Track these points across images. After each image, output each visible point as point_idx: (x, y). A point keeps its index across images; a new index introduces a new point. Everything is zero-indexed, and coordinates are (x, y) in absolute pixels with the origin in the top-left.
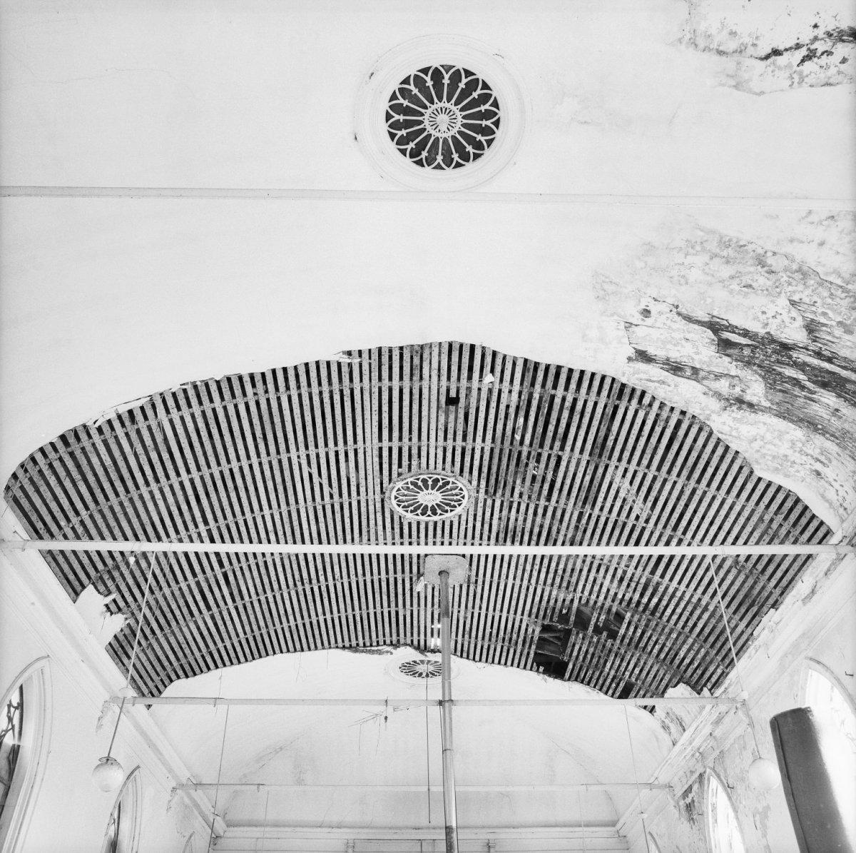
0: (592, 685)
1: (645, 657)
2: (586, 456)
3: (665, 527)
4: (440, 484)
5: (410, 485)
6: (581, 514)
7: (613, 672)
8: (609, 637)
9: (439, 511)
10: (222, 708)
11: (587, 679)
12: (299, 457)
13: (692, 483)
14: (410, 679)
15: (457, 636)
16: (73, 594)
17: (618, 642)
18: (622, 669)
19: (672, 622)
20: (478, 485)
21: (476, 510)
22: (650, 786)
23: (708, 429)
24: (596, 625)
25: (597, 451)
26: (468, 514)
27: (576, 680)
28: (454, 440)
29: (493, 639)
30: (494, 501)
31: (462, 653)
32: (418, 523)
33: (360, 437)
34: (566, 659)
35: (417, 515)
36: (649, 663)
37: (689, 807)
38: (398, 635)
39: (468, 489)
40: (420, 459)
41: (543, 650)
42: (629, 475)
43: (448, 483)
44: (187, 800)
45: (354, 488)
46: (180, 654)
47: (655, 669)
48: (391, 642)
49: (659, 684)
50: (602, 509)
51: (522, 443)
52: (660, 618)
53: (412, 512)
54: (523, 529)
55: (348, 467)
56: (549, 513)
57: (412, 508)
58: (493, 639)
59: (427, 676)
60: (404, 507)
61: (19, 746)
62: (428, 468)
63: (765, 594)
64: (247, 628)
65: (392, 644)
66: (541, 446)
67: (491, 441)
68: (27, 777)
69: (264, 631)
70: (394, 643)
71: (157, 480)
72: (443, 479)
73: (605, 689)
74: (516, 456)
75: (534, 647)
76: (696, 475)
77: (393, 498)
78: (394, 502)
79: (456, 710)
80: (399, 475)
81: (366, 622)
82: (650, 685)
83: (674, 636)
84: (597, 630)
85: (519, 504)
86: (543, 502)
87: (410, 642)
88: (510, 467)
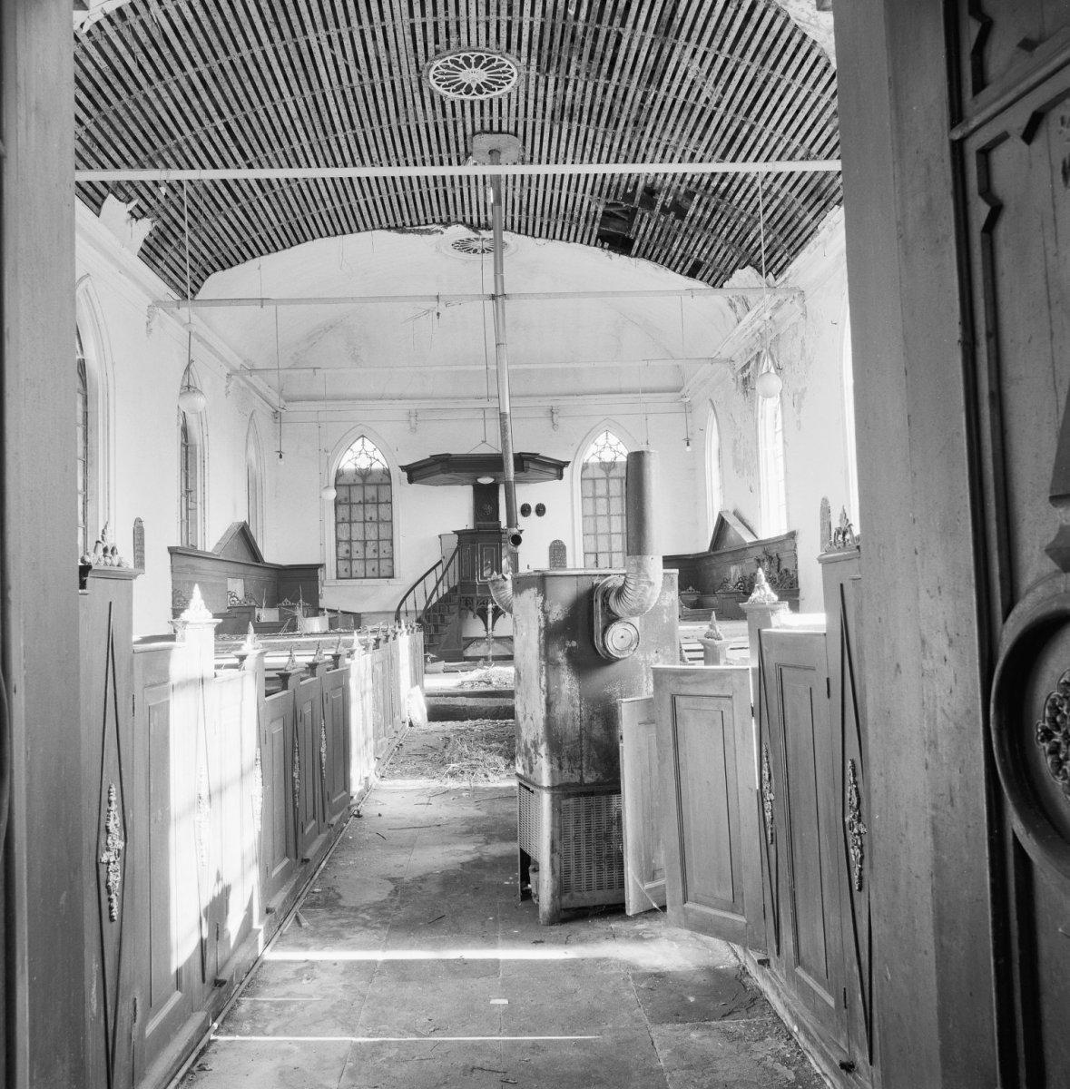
0: (660, 261)
1: (713, 239)
2: (650, 34)
3: (737, 111)
4: (485, 61)
5: (450, 64)
6: (645, 94)
7: (681, 251)
8: (677, 217)
9: (485, 90)
10: (269, 308)
11: (654, 257)
12: (318, 39)
13: (767, 69)
14: (464, 255)
15: (513, 212)
16: (95, 208)
17: (686, 222)
18: (691, 248)
19: (742, 207)
20: (529, 62)
21: (527, 87)
22: (712, 360)
23: (785, 14)
24: (663, 205)
25: (662, 29)
26: (518, 92)
27: (643, 256)
28: (498, 14)
29: (554, 216)
30: (547, 78)
31: (523, 229)
32: (463, 102)
33: (387, 15)
34: (632, 236)
35: (461, 94)
36: (718, 245)
37: (745, 381)
38: (448, 212)
39: (517, 71)
40: (460, 37)
41: (608, 227)
42: (698, 57)
43: (494, 60)
44: (242, 383)
45: (385, 69)
46: (214, 248)
47: (723, 250)
48: (441, 220)
49: (729, 263)
50: (668, 90)
51: (577, 17)
52: (731, 201)
53: (453, 91)
54: (582, 108)
55: (376, 47)
56: (610, 93)
57: (454, 87)
58: (554, 216)
59: (483, 251)
60: (444, 86)
61: (84, 360)
62: (469, 44)
63: (833, 189)
64: (282, 217)
65: (441, 222)
66: (599, 21)
67: (540, 15)
68: (100, 387)
69: (300, 218)
70: (444, 221)
71: (160, 77)
72: (487, 57)
73: (673, 266)
74: (570, 32)
75: (597, 224)
76: (771, 61)
77: (431, 77)
78: (433, 82)
79: (509, 305)
80: (437, 52)
81: (411, 203)
82: (719, 264)
83: (744, 220)
84: (664, 210)
85: (576, 81)
86: (602, 81)
87: (462, 220)
88: (564, 43)
